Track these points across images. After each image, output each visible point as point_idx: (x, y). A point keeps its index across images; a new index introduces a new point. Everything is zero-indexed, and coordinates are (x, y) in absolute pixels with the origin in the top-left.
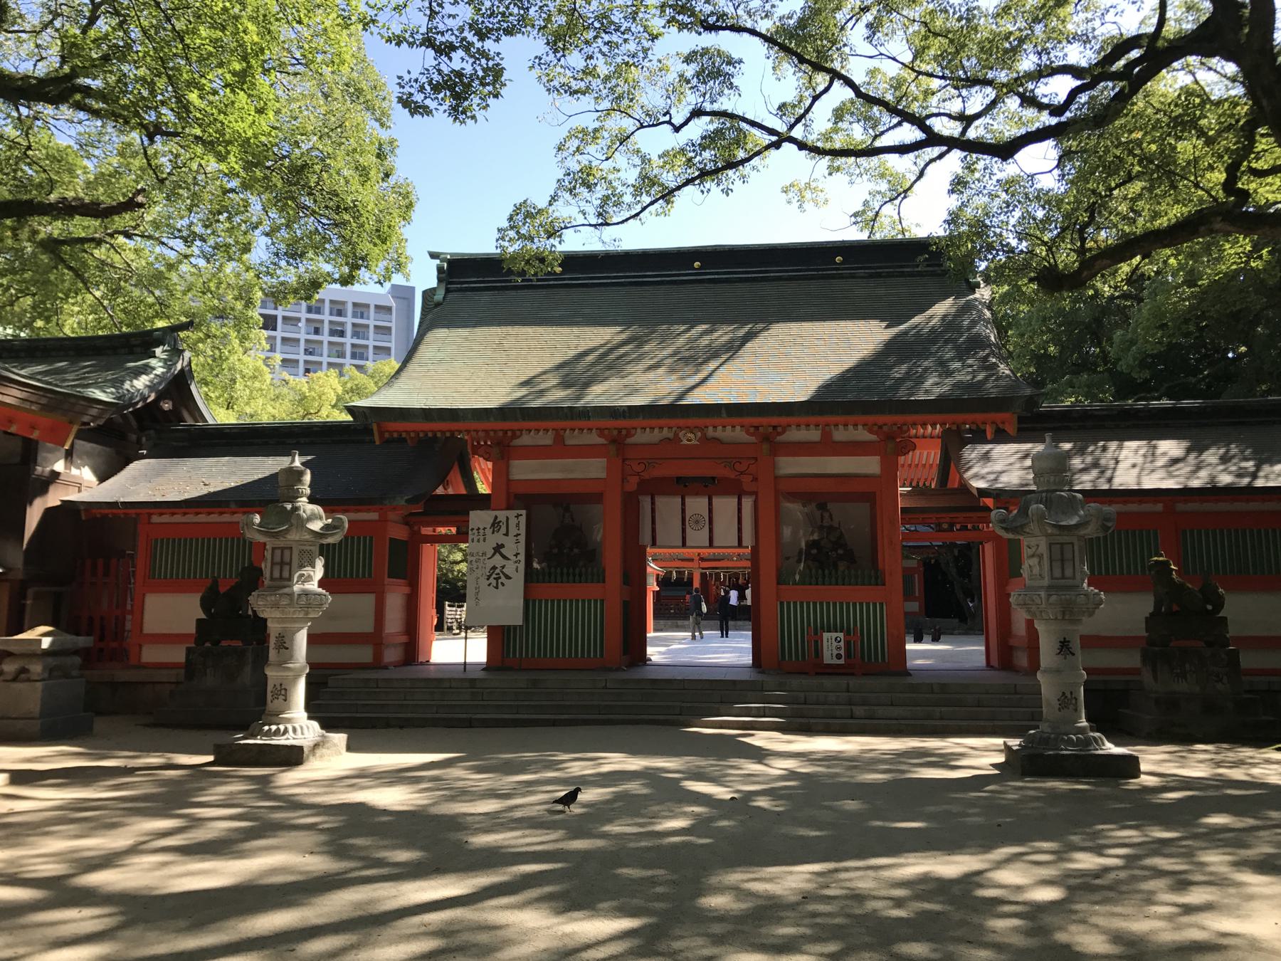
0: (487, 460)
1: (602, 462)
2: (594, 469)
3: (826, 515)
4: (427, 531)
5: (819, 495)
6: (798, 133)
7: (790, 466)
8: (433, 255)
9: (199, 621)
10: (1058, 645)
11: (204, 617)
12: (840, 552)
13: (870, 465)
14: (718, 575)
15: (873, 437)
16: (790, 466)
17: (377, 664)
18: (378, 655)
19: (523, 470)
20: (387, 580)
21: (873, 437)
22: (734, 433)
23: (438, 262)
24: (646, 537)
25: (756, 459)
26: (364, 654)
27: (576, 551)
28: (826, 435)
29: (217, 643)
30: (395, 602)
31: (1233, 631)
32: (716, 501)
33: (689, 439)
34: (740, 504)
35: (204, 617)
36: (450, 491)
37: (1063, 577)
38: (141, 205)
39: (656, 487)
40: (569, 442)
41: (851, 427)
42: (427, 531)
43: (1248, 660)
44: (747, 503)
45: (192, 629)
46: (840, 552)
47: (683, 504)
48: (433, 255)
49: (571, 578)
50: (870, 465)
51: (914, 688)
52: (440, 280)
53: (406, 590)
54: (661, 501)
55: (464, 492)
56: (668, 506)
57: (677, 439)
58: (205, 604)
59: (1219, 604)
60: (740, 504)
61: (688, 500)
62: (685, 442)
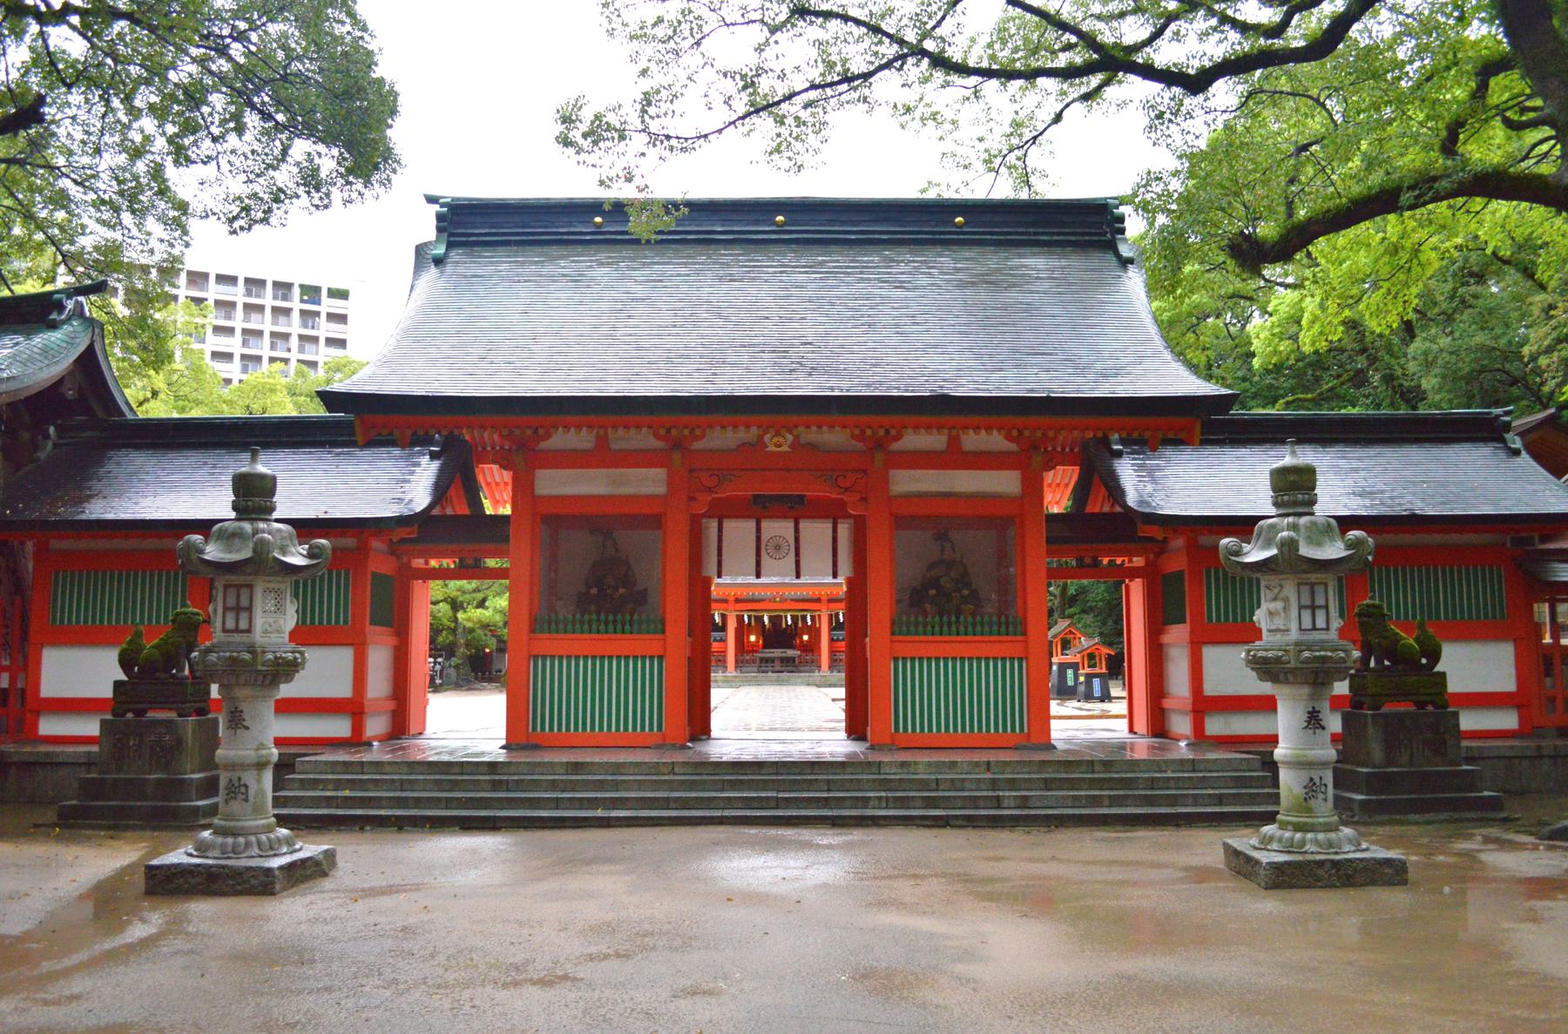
0: (503, 467)
1: (660, 473)
2: (649, 482)
3: (948, 545)
4: (418, 563)
5: (939, 518)
6: (929, 45)
7: (907, 482)
8: (431, 200)
9: (117, 684)
10: (1305, 717)
11: (124, 678)
12: (966, 592)
13: (1006, 482)
14: (804, 618)
15: (1013, 447)
16: (907, 482)
17: (357, 740)
18: (358, 728)
19: (553, 483)
20: (370, 629)
21: (1013, 447)
22: (834, 437)
23: (437, 207)
24: (711, 569)
25: (865, 471)
26: (339, 727)
27: (622, 591)
28: (954, 442)
29: (140, 713)
30: (379, 660)
31: (1453, 686)
32: (803, 524)
33: (778, 444)
34: (835, 531)
35: (124, 678)
36: (449, 511)
37: (1314, 628)
38: (186, 93)
39: (725, 510)
40: (615, 446)
41: (814, 428)
42: (418, 563)
43: (1469, 721)
44: (844, 529)
45: (108, 693)
46: (966, 592)
47: (758, 530)
48: (431, 200)
49: (611, 627)
50: (1006, 482)
51: (1068, 765)
52: (440, 230)
53: (393, 641)
54: (729, 525)
55: (467, 512)
56: (739, 531)
57: (760, 443)
58: (125, 663)
59: (1435, 656)
60: (835, 531)
61: (765, 524)
62: (772, 448)
